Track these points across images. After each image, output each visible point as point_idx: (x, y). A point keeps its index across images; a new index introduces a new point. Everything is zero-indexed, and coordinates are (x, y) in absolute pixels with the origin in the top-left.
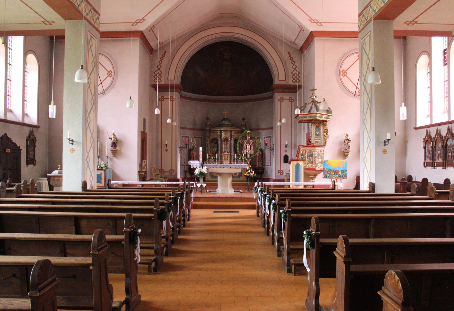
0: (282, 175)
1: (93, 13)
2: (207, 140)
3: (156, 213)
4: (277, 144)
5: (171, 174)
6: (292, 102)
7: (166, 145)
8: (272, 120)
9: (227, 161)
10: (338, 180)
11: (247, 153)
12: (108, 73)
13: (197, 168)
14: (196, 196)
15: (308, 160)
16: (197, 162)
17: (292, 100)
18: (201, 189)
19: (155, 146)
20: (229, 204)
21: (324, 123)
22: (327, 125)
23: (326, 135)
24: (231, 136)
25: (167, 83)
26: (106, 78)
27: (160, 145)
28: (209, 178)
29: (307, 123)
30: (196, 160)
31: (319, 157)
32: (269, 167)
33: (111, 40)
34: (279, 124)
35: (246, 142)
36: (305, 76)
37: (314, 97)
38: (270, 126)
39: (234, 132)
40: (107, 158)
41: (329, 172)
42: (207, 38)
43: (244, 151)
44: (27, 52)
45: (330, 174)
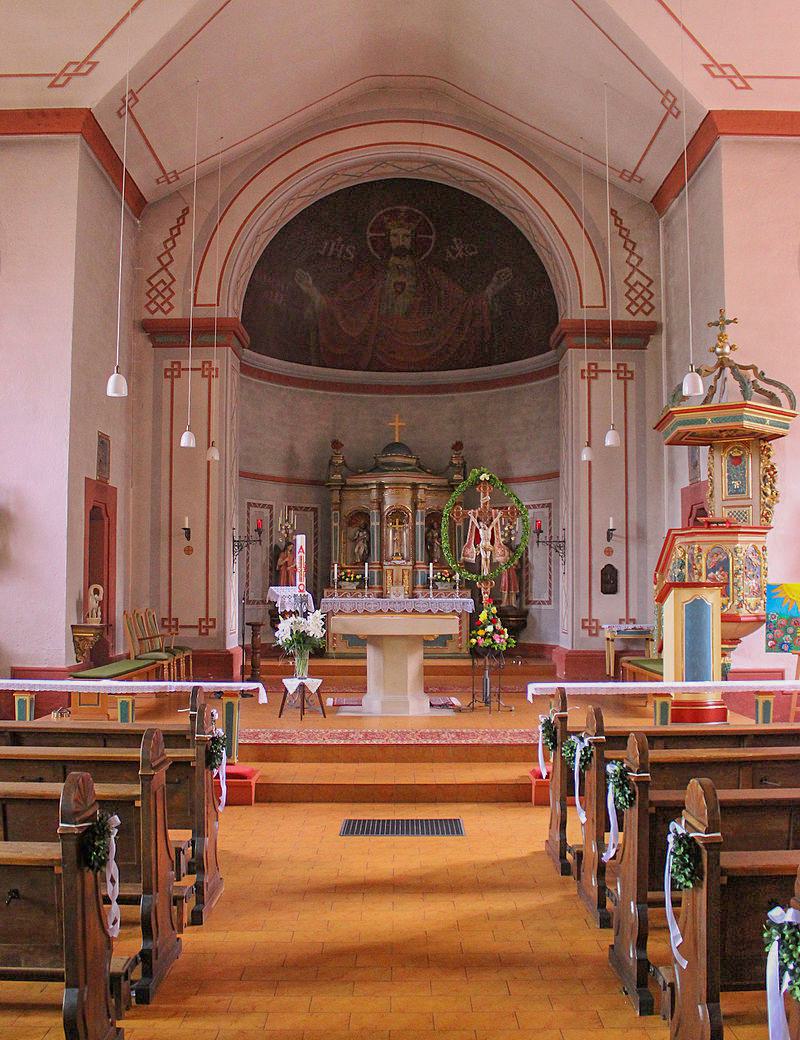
0: (596, 635)
2: (333, 517)
6: (629, 382)
9: (401, 588)
19: (147, 538)
21: (761, 441)
22: (771, 453)
23: (769, 493)
27: (165, 532)
32: (543, 607)
35: (474, 514)
36: (672, 290)
37: (727, 349)
38: (547, 470)
41: (791, 630)
43: (469, 551)
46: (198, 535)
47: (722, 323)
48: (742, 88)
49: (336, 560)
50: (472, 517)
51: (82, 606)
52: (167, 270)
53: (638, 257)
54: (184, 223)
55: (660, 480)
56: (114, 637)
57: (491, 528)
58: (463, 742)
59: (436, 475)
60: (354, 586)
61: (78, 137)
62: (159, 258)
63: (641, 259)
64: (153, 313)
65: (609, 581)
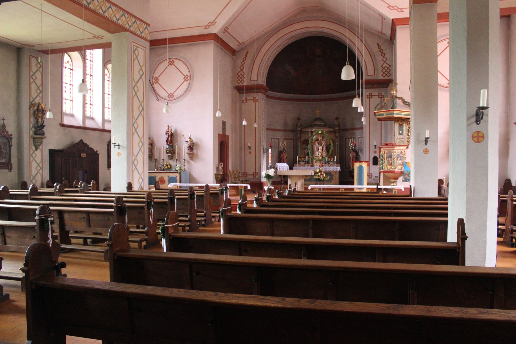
1: (138, 24)
5: (254, 177)
7: (250, 148)
12: (184, 78)
15: (387, 161)
17: (382, 97)
19: (238, 148)
26: (183, 83)
27: (243, 148)
33: (187, 44)
35: (317, 143)
44: (106, 63)
51: (218, 169)
53: (386, 58)
61: (213, 41)
62: (240, 67)
63: (387, 59)
64: (239, 84)
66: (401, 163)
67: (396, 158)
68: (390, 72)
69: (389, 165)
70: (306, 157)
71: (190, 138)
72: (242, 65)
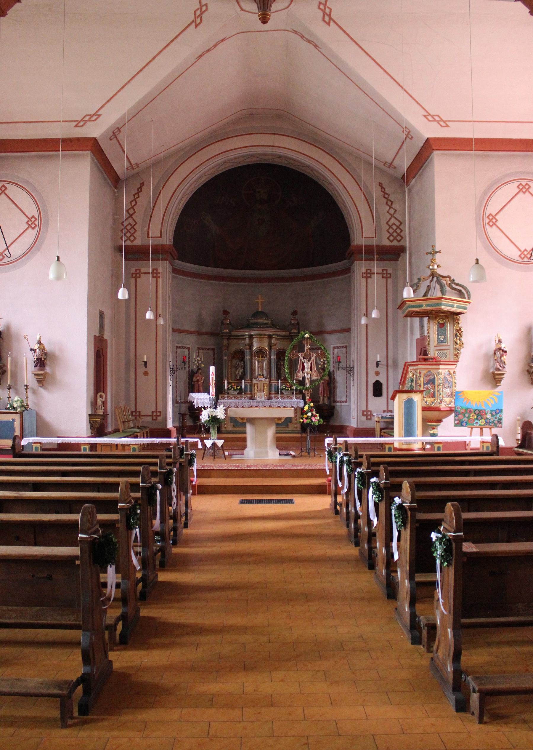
0: (370, 419)
3: (86, 547)
4: (360, 361)
5: (154, 420)
7: (146, 364)
8: (350, 313)
9: (263, 394)
10: (484, 429)
11: (304, 378)
13: (205, 408)
14: (203, 466)
16: (205, 396)
18: (214, 450)
20: (274, 484)
21: (454, 316)
23: (458, 342)
24: (270, 347)
25: (145, 243)
28: (230, 427)
29: (418, 319)
30: (204, 392)
31: (446, 385)
32: (343, 404)
34: (363, 321)
35: (302, 355)
36: (412, 229)
37: (436, 267)
38: (345, 327)
39: (276, 338)
40: (26, 389)
42: (222, 156)
43: (299, 374)
45: (468, 417)
46: (151, 368)
47: (434, 253)
48: (444, 126)
49: (225, 378)
50: (301, 357)
52: (132, 218)
53: (394, 209)
54: (141, 191)
55: (405, 331)
56: (107, 422)
57: (310, 362)
58: (295, 468)
59: (283, 329)
60: (236, 393)
61: (89, 152)
63: (395, 211)
65: (378, 389)
66: (448, 393)
67: (441, 385)
68: (401, 234)
69: (429, 397)
70: (242, 383)
71: (40, 343)
72: (130, 206)
